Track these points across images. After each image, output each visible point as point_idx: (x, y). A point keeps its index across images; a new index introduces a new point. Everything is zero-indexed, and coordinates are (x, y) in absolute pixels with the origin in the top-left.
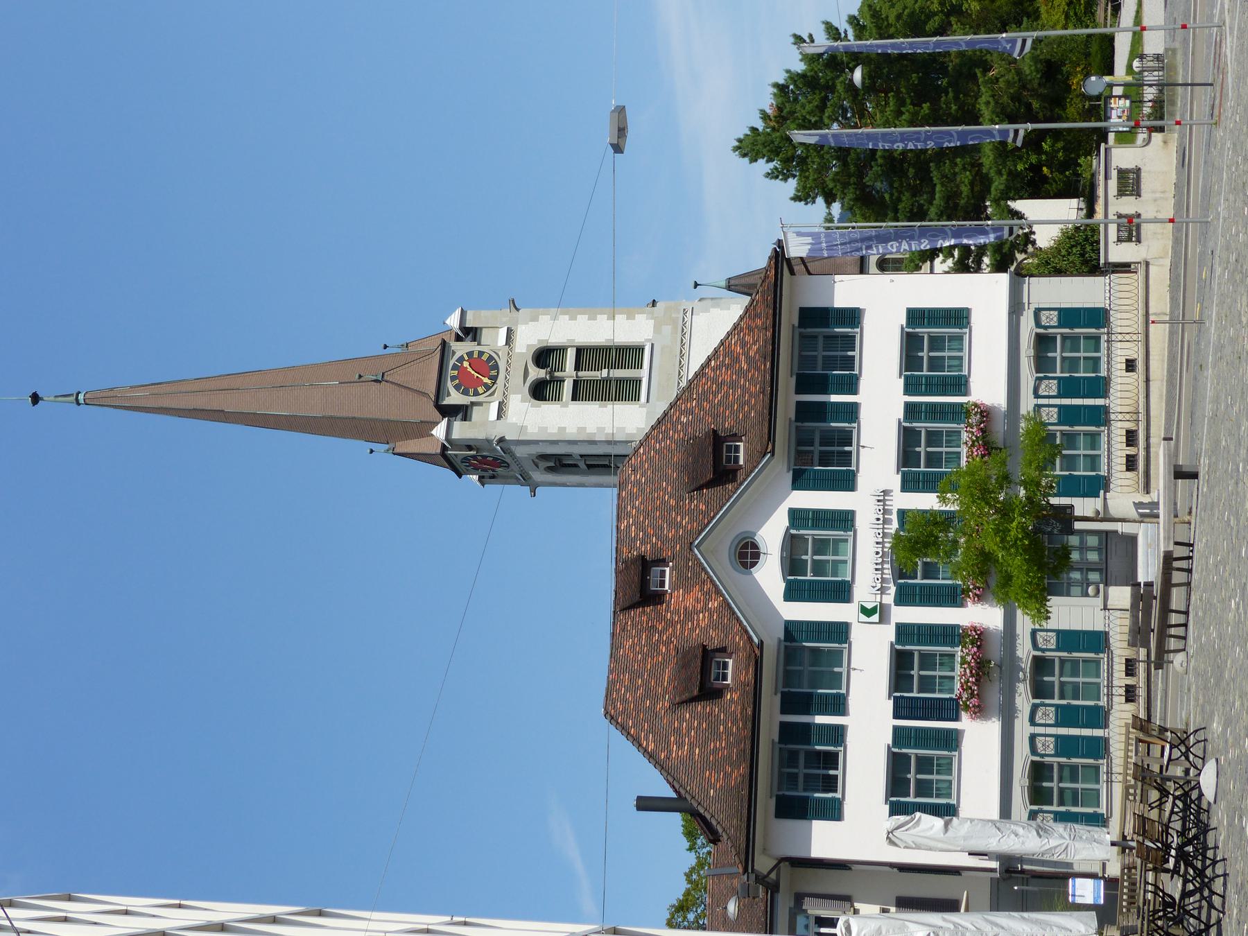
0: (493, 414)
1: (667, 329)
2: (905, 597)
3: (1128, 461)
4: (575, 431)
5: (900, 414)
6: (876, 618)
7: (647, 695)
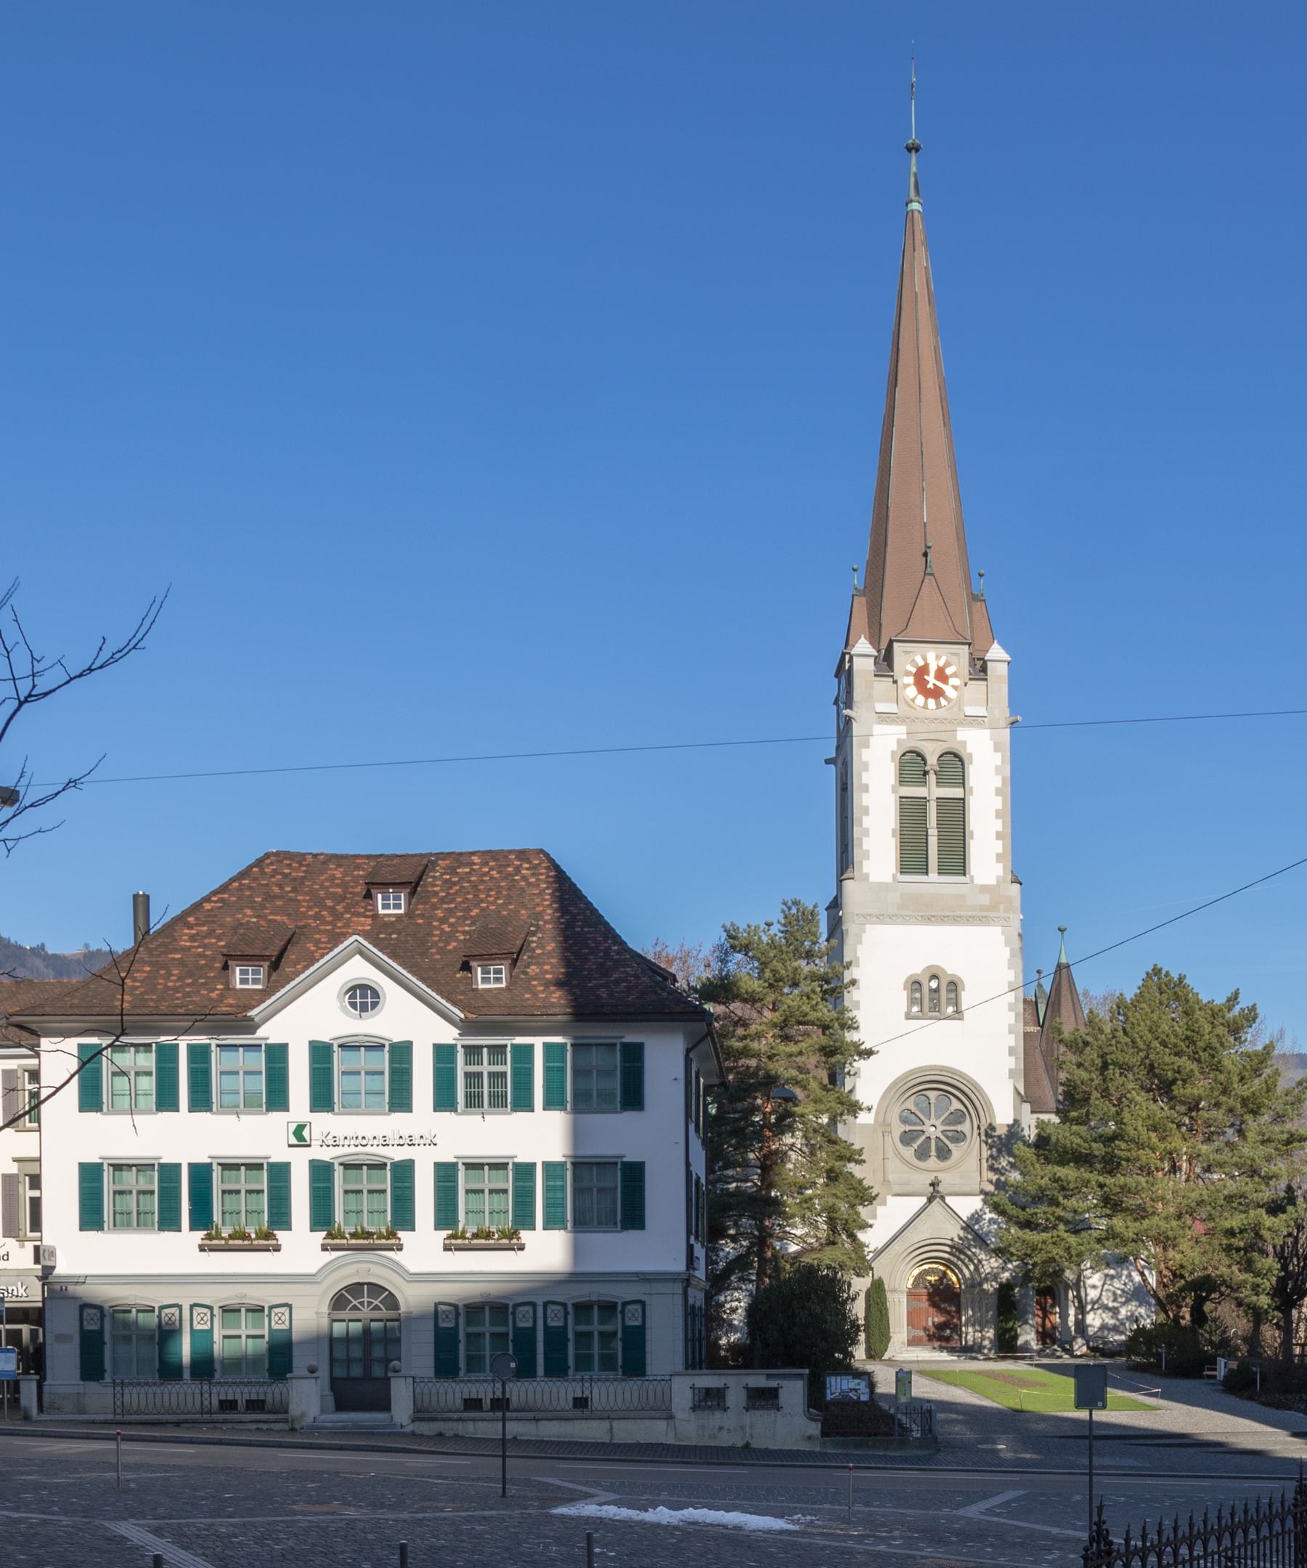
0: (880, 707)
1: (985, 900)
2: (321, 1172)
3: (231, 1401)
4: (864, 803)
5: (521, 1159)
6: (294, 1141)
7: (269, 897)
